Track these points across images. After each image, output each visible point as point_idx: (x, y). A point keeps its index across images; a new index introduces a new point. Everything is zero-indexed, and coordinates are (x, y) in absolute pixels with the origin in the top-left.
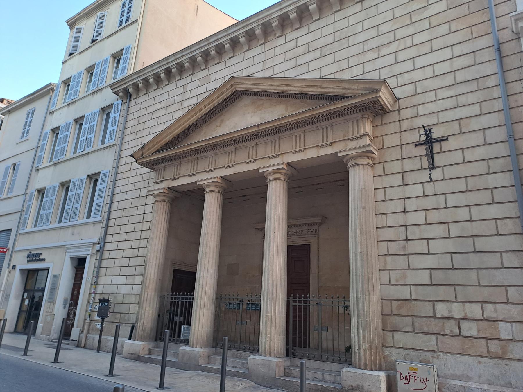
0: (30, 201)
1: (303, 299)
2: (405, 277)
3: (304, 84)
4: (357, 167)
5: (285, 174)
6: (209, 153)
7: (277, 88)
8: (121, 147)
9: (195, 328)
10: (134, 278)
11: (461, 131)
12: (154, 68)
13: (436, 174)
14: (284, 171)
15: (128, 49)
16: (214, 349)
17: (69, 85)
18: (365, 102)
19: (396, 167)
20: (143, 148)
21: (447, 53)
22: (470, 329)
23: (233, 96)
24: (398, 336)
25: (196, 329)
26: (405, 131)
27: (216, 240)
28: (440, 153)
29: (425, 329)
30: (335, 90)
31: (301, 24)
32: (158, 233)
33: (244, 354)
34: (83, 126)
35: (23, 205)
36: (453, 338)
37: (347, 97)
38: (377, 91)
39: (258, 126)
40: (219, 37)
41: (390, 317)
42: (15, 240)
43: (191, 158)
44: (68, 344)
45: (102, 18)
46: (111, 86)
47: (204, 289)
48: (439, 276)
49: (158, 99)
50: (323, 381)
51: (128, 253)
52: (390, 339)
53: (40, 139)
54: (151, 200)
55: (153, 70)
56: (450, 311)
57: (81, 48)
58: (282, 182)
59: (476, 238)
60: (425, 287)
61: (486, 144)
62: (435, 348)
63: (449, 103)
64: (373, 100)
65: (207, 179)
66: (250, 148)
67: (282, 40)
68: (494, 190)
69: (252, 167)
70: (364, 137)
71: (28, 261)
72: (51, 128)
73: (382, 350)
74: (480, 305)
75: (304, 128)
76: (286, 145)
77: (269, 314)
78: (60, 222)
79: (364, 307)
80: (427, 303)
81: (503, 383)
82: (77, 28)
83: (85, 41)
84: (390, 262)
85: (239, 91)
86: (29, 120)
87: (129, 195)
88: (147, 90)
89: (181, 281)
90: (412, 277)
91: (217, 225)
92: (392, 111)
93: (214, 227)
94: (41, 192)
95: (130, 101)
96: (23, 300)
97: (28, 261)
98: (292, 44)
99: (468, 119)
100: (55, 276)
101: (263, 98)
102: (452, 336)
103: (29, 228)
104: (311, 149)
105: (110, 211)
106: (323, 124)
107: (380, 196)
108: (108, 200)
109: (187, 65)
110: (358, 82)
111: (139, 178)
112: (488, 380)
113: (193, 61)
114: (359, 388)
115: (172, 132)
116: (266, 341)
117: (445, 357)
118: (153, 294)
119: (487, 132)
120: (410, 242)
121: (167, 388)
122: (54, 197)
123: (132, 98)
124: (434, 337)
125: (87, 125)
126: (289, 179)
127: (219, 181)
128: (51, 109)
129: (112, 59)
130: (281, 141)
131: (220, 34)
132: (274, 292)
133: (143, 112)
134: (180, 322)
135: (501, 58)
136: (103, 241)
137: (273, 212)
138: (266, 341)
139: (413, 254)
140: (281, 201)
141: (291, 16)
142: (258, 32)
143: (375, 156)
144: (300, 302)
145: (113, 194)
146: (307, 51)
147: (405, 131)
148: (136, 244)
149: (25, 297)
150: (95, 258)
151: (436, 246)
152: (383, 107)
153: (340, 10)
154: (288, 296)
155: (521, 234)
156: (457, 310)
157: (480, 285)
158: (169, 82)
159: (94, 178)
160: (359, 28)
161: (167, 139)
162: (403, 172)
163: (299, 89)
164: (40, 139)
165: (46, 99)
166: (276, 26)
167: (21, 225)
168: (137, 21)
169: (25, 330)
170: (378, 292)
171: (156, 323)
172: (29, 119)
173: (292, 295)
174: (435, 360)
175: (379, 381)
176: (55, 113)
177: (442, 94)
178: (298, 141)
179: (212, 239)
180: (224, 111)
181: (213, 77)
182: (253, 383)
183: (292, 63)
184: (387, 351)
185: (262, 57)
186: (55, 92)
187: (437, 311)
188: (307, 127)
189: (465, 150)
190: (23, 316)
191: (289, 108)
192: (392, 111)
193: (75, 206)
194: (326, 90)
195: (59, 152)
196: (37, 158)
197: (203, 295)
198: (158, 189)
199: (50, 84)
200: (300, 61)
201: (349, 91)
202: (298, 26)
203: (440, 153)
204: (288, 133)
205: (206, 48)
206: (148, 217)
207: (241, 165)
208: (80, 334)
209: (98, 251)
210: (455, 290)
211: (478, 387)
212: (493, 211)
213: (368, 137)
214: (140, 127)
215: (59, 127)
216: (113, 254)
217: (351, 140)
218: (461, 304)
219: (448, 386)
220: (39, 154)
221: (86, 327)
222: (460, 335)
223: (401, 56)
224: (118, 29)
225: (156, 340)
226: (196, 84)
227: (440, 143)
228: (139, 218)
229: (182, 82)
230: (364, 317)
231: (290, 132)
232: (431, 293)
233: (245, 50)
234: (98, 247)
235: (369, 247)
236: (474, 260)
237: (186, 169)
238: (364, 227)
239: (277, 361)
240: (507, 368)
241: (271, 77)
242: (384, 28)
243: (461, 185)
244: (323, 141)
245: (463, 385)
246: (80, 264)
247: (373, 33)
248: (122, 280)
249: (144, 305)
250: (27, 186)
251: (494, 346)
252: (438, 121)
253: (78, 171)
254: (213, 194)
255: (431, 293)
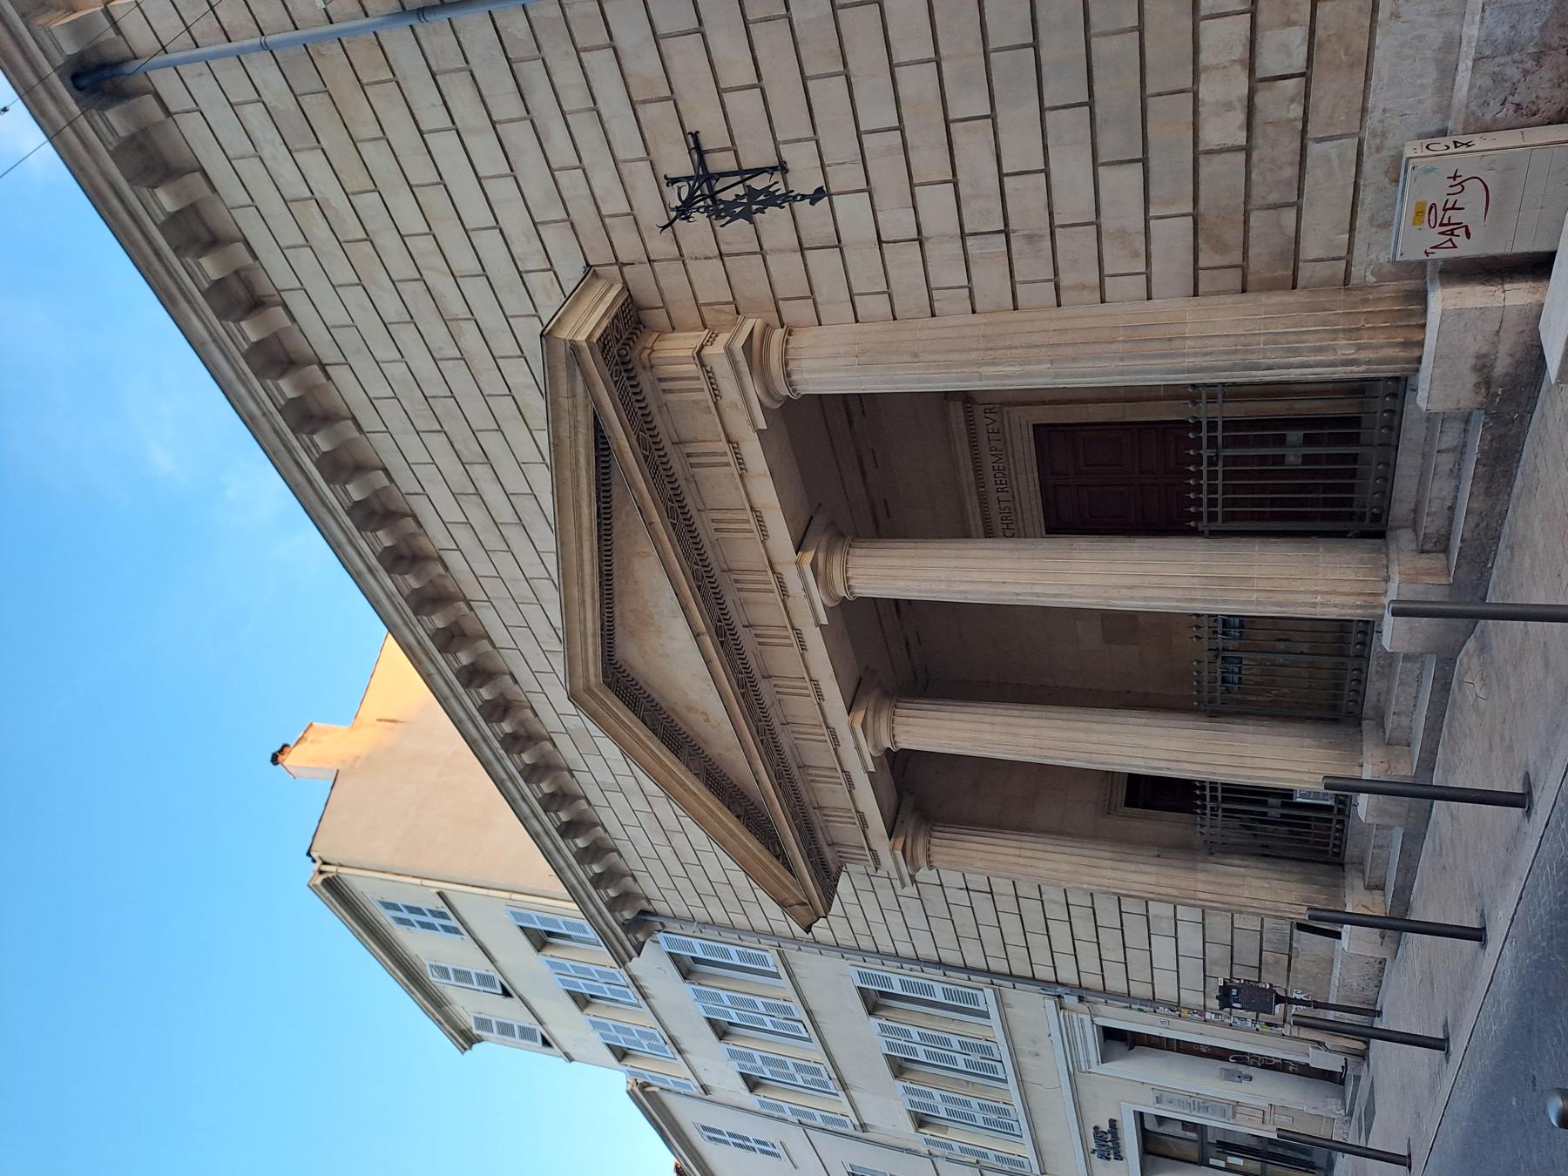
2: (1122, 234)
3: (571, 528)
4: (794, 377)
5: (829, 552)
6: (784, 740)
7: (588, 589)
9: (1300, 781)
11: (667, 99)
12: (563, 864)
14: (821, 557)
16: (1365, 723)
18: (608, 374)
19: (786, 269)
23: (622, 689)
24: (1311, 247)
25: (1306, 777)
26: (679, 247)
28: (736, 152)
29: (1290, 172)
32: (1021, 861)
36: (1314, 94)
38: (574, 348)
43: (800, 785)
45: (444, 972)
48: (1116, 141)
50: (1461, 450)
51: (1084, 929)
52: (1323, 270)
55: (569, 867)
56: (1228, 106)
58: (853, 561)
59: (992, 45)
60: (1153, 177)
64: (599, 354)
65: (858, 748)
70: (706, 361)
71: (1119, 1157)
72: (747, 1093)
73: (1357, 289)
74: (1202, 24)
75: (693, 512)
77: (1255, 596)
79: (1225, 353)
80: (1203, 173)
83: (511, 1012)
85: (605, 675)
86: (731, 1140)
88: (624, 876)
90: (1124, 211)
91: (988, 719)
92: (625, 282)
93: (997, 728)
95: (655, 914)
97: (1119, 1157)
98: (464, 536)
100: (1158, 1100)
101: (617, 613)
102: (1307, 96)
104: (751, 495)
106: (677, 465)
107: (874, 306)
108: (937, 974)
109: (546, 787)
111: (868, 899)
114: (1484, 366)
115: (733, 835)
116: (1335, 606)
117: (1377, 114)
118: (1201, 876)
119: (662, 29)
120: (1013, 224)
121: (1482, 915)
122: (936, 1094)
123: (649, 908)
124: (1314, 149)
126: (842, 535)
127: (860, 716)
128: (697, 1091)
129: (548, 952)
130: (733, 565)
132: (1185, 583)
133: (683, 884)
134: (1284, 805)
136: (1053, 987)
137: (943, 586)
138: (1335, 606)
139: (1051, 215)
140: (908, 563)
141: (388, 543)
142: (439, 621)
143: (759, 323)
145: (918, 960)
146: (476, 498)
147: (679, 247)
149: (1222, 1164)
151: (1021, 149)
152: (616, 316)
153: (354, 419)
154: (1194, 533)
156: (1223, 88)
159: (875, 1002)
160: (397, 371)
161: (754, 845)
162: (802, 249)
163: (586, 537)
165: (672, 1102)
166: (417, 578)
168: (441, 895)
170: (1173, 307)
171: (1287, 866)
173: (1192, 509)
174: (1390, 143)
175: (1460, 313)
177: (561, 152)
178: (736, 526)
179: (1033, 731)
180: (664, 705)
187: (1230, 142)
188: (691, 507)
192: (625, 282)
193: (957, 1047)
194: (583, 474)
195: (809, 1077)
197: (1199, 758)
199: (631, 1093)
200: (504, 513)
201: (581, 418)
202: (409, 524)
203: (736, 152)
204: (710, 553)
205: (497, 744)
206: (977, 881)
207: (811, 665)
209: (1081, 999)
210: (1160, 94)
211: (1478, 18)
214: (725, 893)
215: (745, 1077)
216: (1089, 963)
217: (716, 393)
218: (1203, 77)
219: (1473, 106)
220: (819, 1123)
222: (1306, 75)
223: (464, 261)
225: (1342, 865)
227: (708, 152)
228: (983, 904)
229: (594, 795)
230: (1253, 352)
231: (708, 547)
232: (1171, 161)
234: (1071, 1001)
235: (1036, 338)
237: (832, 795)
238: (974, 355)
241: (544, 395)
242: (391, 307)
243: (829, 93)
244: (727, 464)
245: (1470, 64)
246: (1115, 1040)
248: (1163, 949)
249: (1235, 900)
250: (908, 1151)
252: (641, 160)
253: (862, 1041)
254: (898, 729)
255: (1171, 161)
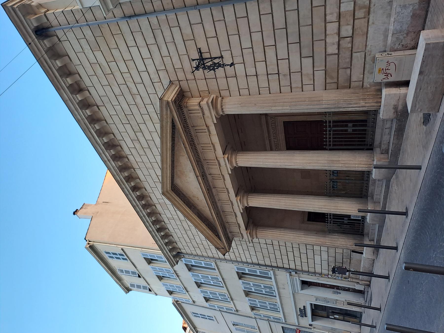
0: (260, 315)
1: (328, 140)
5: (232, 154)
6: (219, 204)
8: (217, 259)
9: (352, 213)
10: (315, 250)
11: (193, 40)
12: (157, 239)
13: (227, 60)
14: (230, 156)
15: (143, 255)
17: (163, 277)
20: (218, 249)
21: (134, 50)
22: (347, 31)
23: (176, 192)
24: (354, 78)
27: (284, 199)
28: (210, 53)
29: (348, 60)
30: (168, 129)
31: (118, 146)
32: (281, 236)
33: (379, 124)
34: (194, 264)
35: (264, 320)
37: (172, 120)
38: (168, 103)
39: (197, 177)
40: (132, 199)
41: (339, 84)
42: (290, 325)
44: (368, 292)
45: (122, 271)
46: (172, 266)
47: (322, 207)
48: (305, 52)
49: (180, 235)
50: (391, 128)
51: (297, 254)
52: (357, 84)
53: (214, 309)
54: (255, 240)
56: (334, 44)
57: (145, 284)
61: (202, 23)
62: (363, 54)
63: (172, 48)
65: (238, 206)
66: (196, 132)
67: (131, 157)
68: (237, 16)
69: (213, 129)
71: (306, 316)
72: (205, 302)
76: (210, 155)
78: (270, 278)
80: (327, 60)
81: (389, 7)
82: (131, 286)
83: (141, 282)
84: (296, 84)
86: (200, 316)
87: (253, 253)
89: (315, 220)
91: (272, 198)
92: (180, 85)
94: (253, 309)
95: (182, 253)
96: (335, 319)
97: (306, 316)
98: (133, 151)
99: (183, 35)
102: (352, 42)
103: (281, 315)
104: (212, 139)
105: (266, 265)
108: (257, 267)
109: (153, 219)
110: (162, 116)
111: (240, 247)
112: (387, 17)
113: (145, 207)
114: (396, 108)
115: (205, 230)
117: (369, 46)
118: (327, 239)
119: (192, 22)
122: (257, 300)
123: (180, 251)
124: (354, 55)
125: (202, 280)
127: (239, 198)
128: (191, 302)
129: (151, 265)
130: (206, 158)
131: (99, 151)
133: (190, 245)
135: (136, 15)
136: (288, 270)
137: (261, 163)
139: (290, 69)
143: (215, 96)
144: (330, 141)
145: (252, 263)
146: (138, 141)
148: (290, 249)
149: (333, 317)
150: (302, 275)
151: (282, 54)
153: (106, 120)
155: (271, 1)
156: (332, 39)
157: (312, 25)
158: (166, 229)
161: (210, 233)
162: (226, 77)
164: (214, 309)
165: (184, 305)
166: (121, 162)
167: (279, 321)
168: (122, 249)
169: (358, 318)
170: (320, 93)
172: (199, 315)
174: (372, 53)
176: (194, 300)
177: (165, 52)
178: (201, 131)
179: (284, 201)
181: (161, 201)
182: (394, 177)
183: (148, 151)
184: (366, 84)
185: (144, 170)
186: (178, 300)
188: (196, 143)
189: (207, 37)
190: (346, 318)
191: (181, 154)
192: (180, 85)
193: (263, 287)
196: (228, 311)
197: (327, 207)
198: (248, 237)
199: (173, 304)
201: (169, 120)
204: (200, 155)
205: (141, 207)
206: (269, 241)
208: (360, 284)
209: (296, 273)
212: (254, 17)
213: (201, 103)
217: (203, 114)
218: (327, 37)
220: (225, 310)
221: (354, 280)
222: (352, 37)
224: (129, 261)
225: (363, 235)
226: (167, 212)
227: (203, 53)
228: (270, 247)
229: (166, 220)
230: (340, 104)
233: (139, 181)
234: (293, 273)
235: (286, 100)
236: (293, 29)
237: (231, 219)
238: (270, 104)
239: (376, 160)
240: (376, 5)
243: (234, 39)
244: (206, 132)
246: (305, 284)
247: (121, 99)
250: (249, 317)
251: (360, 14)
253: (237, 286)
